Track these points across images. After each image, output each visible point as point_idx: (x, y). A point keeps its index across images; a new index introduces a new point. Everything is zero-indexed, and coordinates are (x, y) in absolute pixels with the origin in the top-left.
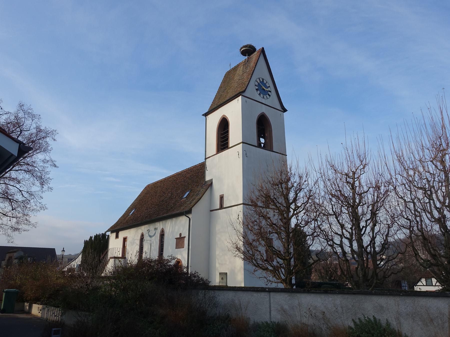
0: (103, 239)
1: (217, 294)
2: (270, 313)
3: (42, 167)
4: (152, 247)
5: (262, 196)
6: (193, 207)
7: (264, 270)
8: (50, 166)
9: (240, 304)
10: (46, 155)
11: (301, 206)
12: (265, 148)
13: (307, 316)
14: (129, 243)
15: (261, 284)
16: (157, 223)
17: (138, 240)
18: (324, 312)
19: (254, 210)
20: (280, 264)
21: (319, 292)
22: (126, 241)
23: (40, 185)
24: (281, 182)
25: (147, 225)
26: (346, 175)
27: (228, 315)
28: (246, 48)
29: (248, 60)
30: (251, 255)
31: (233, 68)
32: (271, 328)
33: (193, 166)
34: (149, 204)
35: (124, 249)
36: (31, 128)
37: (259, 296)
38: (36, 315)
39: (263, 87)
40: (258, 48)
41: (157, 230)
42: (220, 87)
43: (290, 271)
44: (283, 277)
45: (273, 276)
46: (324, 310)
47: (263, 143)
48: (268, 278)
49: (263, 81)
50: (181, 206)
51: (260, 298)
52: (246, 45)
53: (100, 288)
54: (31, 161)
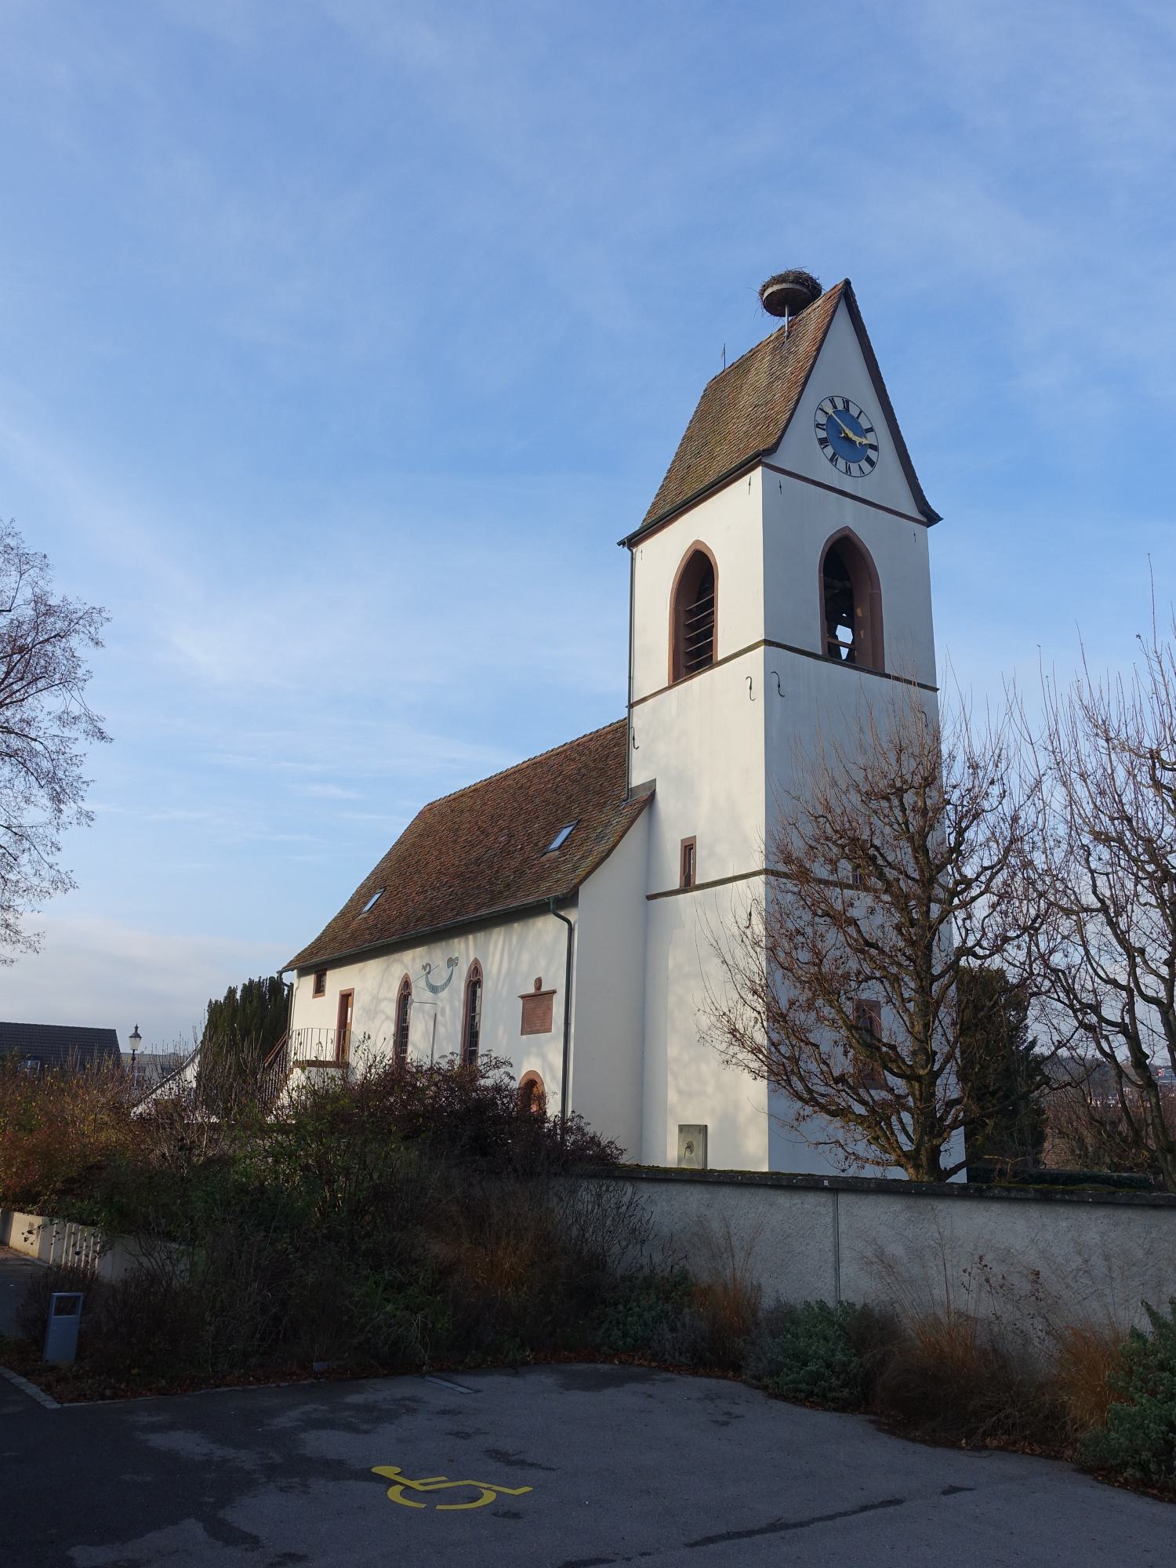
0: (273, 999)
1: (646, 1196)
2: (837, 1269)
3: (56, 740)
4: (441, 1029)
5: (827, 839)
6: (581, 882)
7: (834, 1114)
8: (84, 736)
9: (728, 1233)
10: (68, 696)
11: (976, 879)
12: (854, 663)
13: (974, 1284)
14: (360, 1012)
15: (827, 1166)
16: (456, 940)
17: (390, 1000)
18: (1038, 1273)
19: (796, 889)
20: (898, 1097)
21: (1018, 1196)
22: (349, 1004)
23: (49, 804)
24: (898, 784)
25: (421, 949)
26: (1154, 755)
27: (684, 1276)
28: (784, 286)
29: (789, 333)
30: (784, 1060)
31: (735, 365)
32: (836, 1326)
33: (588, 733)
34: (429, 874)
35: (345, 1032)
36: (18, 601)
37: (799, 1206)
38: (23, 1251)
39: (847, 431)
40: (828, 283)
41: (457, 964)
42: (687, 439)
43: (932, 1123)
44: (907, 1146)
45: (868, 1140)
46: (1040, 1266)
47: (845, 645)
48: (851, 1145)
49: (847, 409)
50: (542, 879)
51: (801, 1214)
52: (781, 275)
53: (232, 1161)
54: (18, 717)
